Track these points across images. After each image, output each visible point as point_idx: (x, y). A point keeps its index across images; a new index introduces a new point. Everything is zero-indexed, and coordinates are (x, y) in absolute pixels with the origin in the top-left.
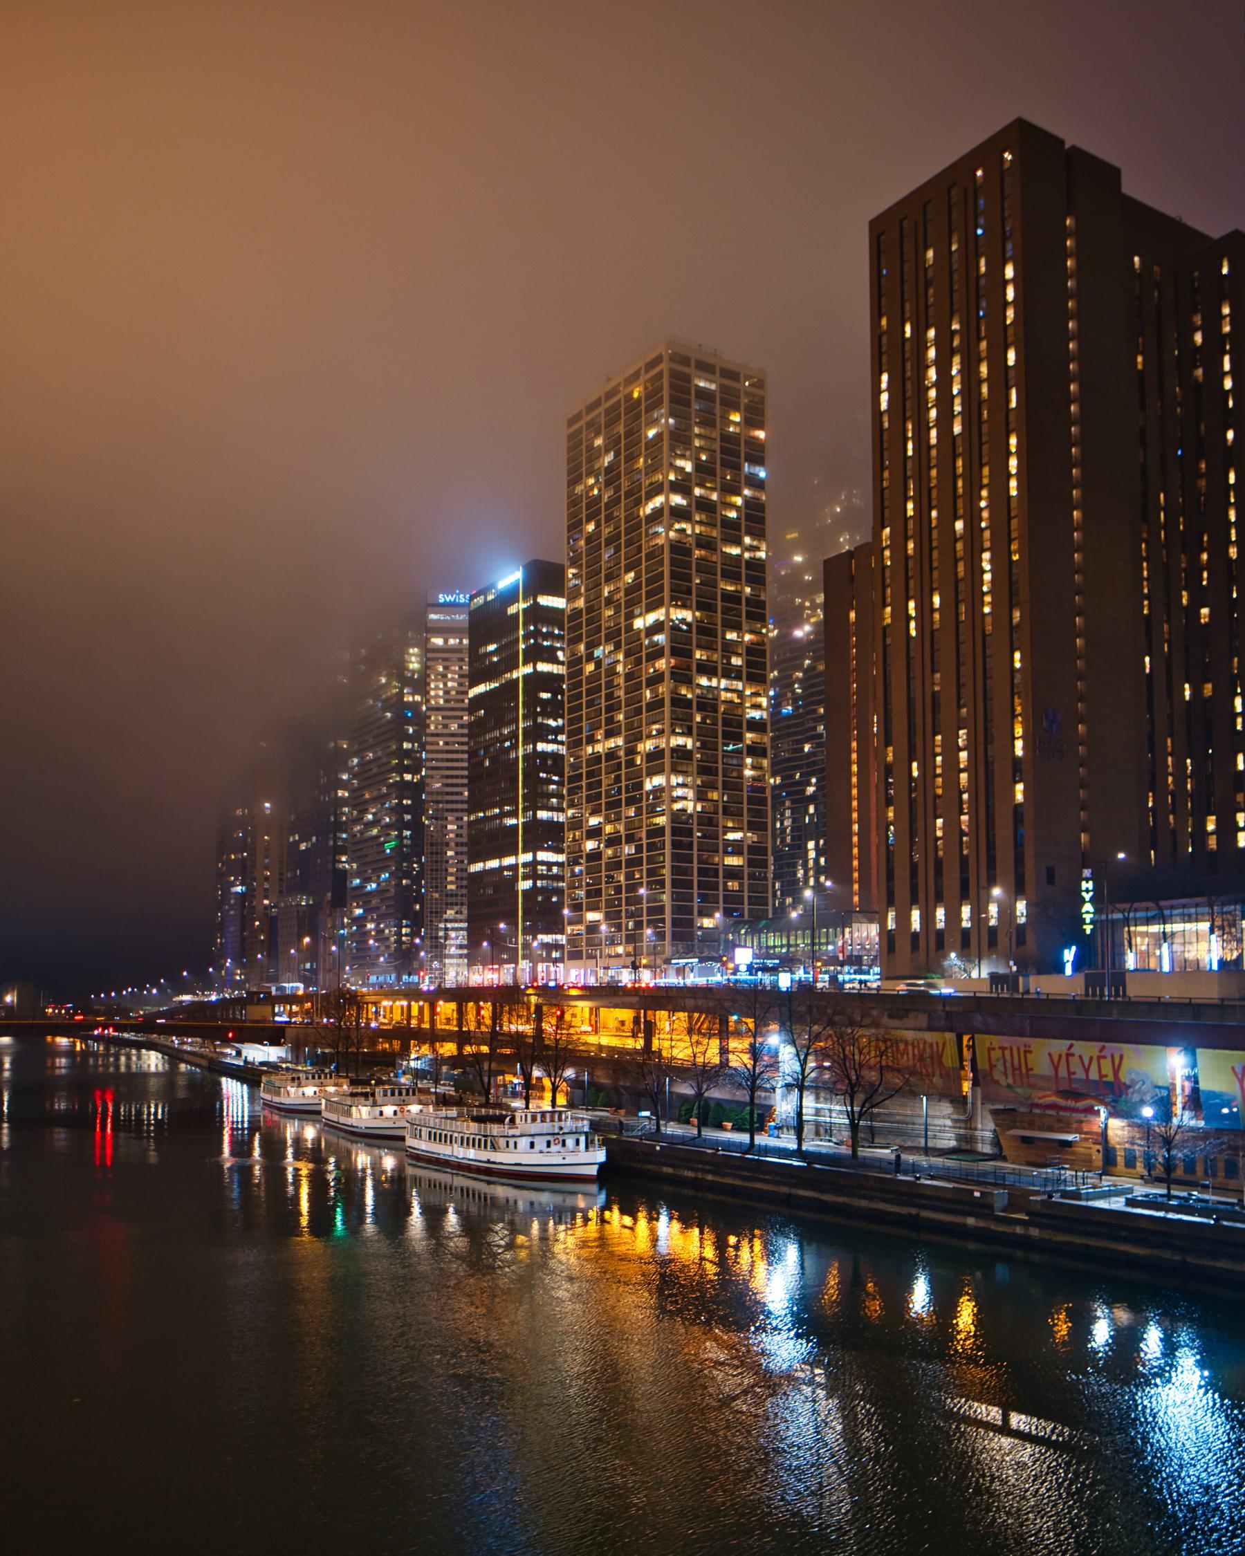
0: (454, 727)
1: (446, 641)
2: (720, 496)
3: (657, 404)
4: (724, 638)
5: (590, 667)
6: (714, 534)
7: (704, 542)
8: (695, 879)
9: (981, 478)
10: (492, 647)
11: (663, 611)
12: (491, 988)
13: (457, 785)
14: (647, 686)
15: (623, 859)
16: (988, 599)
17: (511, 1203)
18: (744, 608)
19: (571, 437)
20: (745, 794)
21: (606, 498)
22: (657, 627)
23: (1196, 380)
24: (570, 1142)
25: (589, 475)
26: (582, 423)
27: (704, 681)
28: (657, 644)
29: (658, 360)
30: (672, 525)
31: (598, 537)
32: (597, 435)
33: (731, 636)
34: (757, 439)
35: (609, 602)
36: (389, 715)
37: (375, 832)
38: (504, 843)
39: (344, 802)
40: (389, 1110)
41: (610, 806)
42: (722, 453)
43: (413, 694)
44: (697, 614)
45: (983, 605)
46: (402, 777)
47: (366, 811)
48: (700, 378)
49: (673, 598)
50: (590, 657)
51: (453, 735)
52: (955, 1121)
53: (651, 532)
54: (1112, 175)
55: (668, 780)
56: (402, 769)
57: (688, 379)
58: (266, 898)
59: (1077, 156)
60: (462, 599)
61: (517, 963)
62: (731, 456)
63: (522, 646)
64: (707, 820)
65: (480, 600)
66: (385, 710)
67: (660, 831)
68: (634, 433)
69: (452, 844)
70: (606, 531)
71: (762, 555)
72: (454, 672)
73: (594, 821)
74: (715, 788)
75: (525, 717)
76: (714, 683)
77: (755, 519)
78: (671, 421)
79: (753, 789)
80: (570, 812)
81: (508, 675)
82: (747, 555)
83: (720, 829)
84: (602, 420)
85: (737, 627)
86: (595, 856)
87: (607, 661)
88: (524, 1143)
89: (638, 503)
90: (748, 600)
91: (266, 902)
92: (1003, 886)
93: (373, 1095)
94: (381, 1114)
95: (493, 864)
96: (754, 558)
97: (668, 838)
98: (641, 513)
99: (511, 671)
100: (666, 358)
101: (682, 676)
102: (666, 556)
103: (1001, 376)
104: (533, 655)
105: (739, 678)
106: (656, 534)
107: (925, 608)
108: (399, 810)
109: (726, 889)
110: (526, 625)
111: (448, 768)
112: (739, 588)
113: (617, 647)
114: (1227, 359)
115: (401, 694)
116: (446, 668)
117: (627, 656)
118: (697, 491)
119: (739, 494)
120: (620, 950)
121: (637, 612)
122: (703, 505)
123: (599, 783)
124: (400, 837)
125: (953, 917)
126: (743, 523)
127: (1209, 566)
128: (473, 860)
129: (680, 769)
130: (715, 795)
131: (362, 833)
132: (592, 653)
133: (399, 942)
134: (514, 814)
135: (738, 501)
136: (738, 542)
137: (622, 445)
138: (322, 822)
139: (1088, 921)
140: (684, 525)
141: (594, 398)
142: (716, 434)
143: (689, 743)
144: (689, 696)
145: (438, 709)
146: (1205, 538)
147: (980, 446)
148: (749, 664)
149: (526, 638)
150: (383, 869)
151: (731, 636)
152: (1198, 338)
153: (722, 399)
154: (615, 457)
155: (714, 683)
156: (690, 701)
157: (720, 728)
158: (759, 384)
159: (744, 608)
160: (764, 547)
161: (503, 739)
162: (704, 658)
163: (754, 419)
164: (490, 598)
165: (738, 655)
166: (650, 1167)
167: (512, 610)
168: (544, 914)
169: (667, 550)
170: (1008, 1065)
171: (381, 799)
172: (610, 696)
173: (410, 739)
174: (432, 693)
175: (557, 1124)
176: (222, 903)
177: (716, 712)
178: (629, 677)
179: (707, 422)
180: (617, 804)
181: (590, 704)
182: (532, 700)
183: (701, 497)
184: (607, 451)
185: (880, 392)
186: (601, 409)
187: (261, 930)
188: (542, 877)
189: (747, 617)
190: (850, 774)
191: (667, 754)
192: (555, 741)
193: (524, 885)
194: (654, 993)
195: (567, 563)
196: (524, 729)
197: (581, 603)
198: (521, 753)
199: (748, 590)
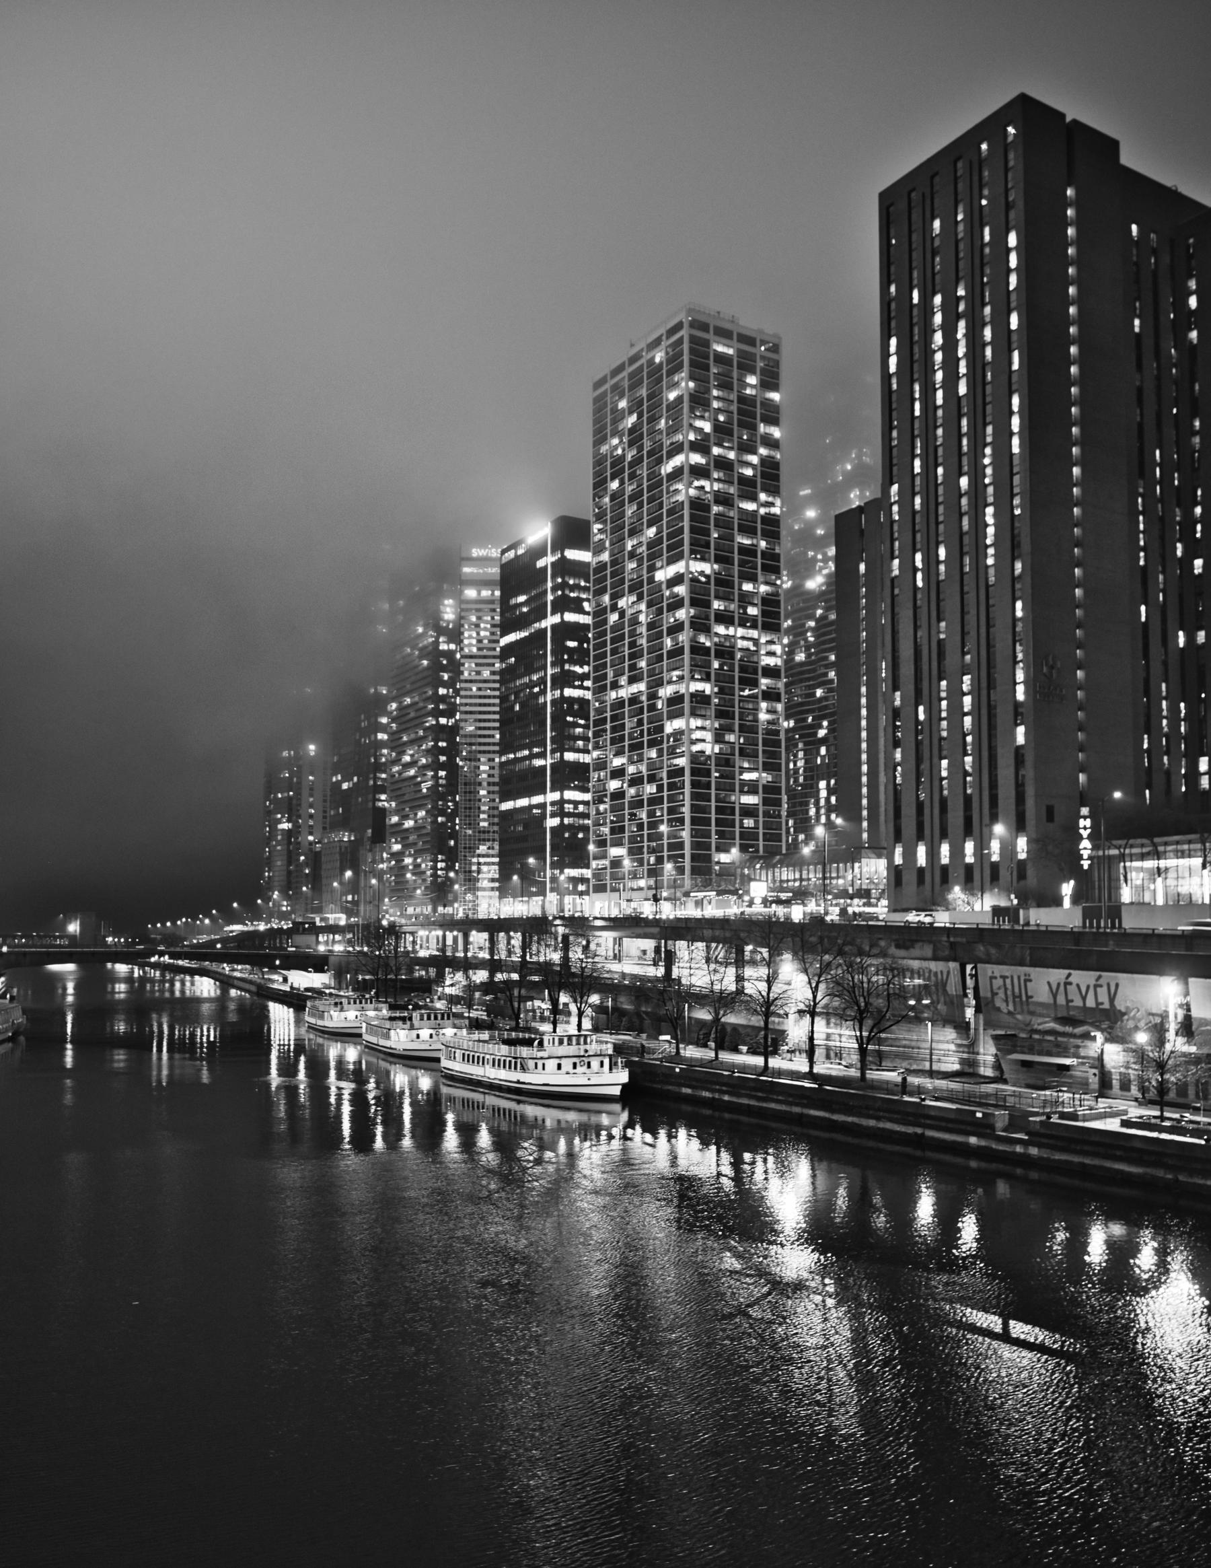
2: (737, 455)
4: (740, 589)
6: (732, 490)
7: (722, 499)
8: (713, 816)
9: (985, 436)
13: (489, 728)
15: (645, 797)
18: (759, 561)
19: (596, 400)
21: (629, 458)
23: (1191, 342)
24: (595, 1063)
25: (613, 436)
26: (607, 386)
27: (721, 629)
29: (679, 326)
30: (691, 483)
32: (621, 397)
35: (632, 555)
37: (412, 772)
38: (532, 782)
40: (425, 1033)
41: (633, 748)
43: (448, 643)
44: (716, 567)
49: (692, 552)
50: (614, 608)
51: (485, 681)
53: (672, 489)
55: (688, 723)
56: (437, 714)
57: (707, 344)
58: (311, 834)
61: (545, 895)
63: (550, 597)
64: (724, 761)
66: (421, 657)
67: (680, 772)
69: (485, 784)
70: (629, 489)
71: (776, 510)
72: (487, 622)
73: (618, 762)
74: (732, 731)
75: (553, 664)
76: (731, 631)
77: (770, 476)
79: (768, 732)
81: (537, 625)
83: (737, 770)
84: (626, 384)
85: (753, 579)
86: (619, 795)
87: (630, 612)
89: (659, 461)
93: (410, 1019)
94: (418, 1036)
95: (523, 802)
97: (687, 778)
98: (663, 472)
100: (686, 325)
101: (700, 625)
102: (686, 512)
103: (1004, 340)
104: (562, 605)
106: (677, 491)
107: (931, 561)
110: (554, 577)
112: (755, 541)
113: (640, 598)
115: (437, 643)
116: (479, 618)
117: (648, 606)
118: (716, 451)
119: (754, 452)
120: (642, 883)
121: (659, 564)
122: (722, 464)
123: (623, 726)
124: (436, 777)
126: (759, 480)
130: (731, 738)
131: (400, 773)
133: (435, 875)
134: (542, 755)
135: (754, 459)
136: (754, 498)
138: (363, 762)
139: (1085, 857)
141: (618, 363)
142: (733, 396)
143: (707, 688)
144: (708, 644)
146: (1199, 493)
147: (983, 406)
148: (764, 613)
149: (554, 589)
150: (420, 807)
151: (748, 587)
153: (738, 363)
155: (731, 631)
156: (709, 649)
158: (775, 349)
159: (759, 561)
160: (778, 502)
162: (722, 608)
164: (520, 552)
166: (670, 1087)
168: (571, 849)
170: (1009, 993)
172: (632, 645)
175: (582, 1047)
176: (270, 839)
177: (733, 658)
178: (651, 626)
179: (725, 385)
180: (639, 746)
181: (614, 652)
182: (559, 649)
184: (631, 413)
186: (625, 374)
187: (306, 864)
188: (569, 815)
189: (763, 569)
191: (687, 699)
192: (581, 687)
193: (552, 822)
195: (592, 519)
197: (605, 557)
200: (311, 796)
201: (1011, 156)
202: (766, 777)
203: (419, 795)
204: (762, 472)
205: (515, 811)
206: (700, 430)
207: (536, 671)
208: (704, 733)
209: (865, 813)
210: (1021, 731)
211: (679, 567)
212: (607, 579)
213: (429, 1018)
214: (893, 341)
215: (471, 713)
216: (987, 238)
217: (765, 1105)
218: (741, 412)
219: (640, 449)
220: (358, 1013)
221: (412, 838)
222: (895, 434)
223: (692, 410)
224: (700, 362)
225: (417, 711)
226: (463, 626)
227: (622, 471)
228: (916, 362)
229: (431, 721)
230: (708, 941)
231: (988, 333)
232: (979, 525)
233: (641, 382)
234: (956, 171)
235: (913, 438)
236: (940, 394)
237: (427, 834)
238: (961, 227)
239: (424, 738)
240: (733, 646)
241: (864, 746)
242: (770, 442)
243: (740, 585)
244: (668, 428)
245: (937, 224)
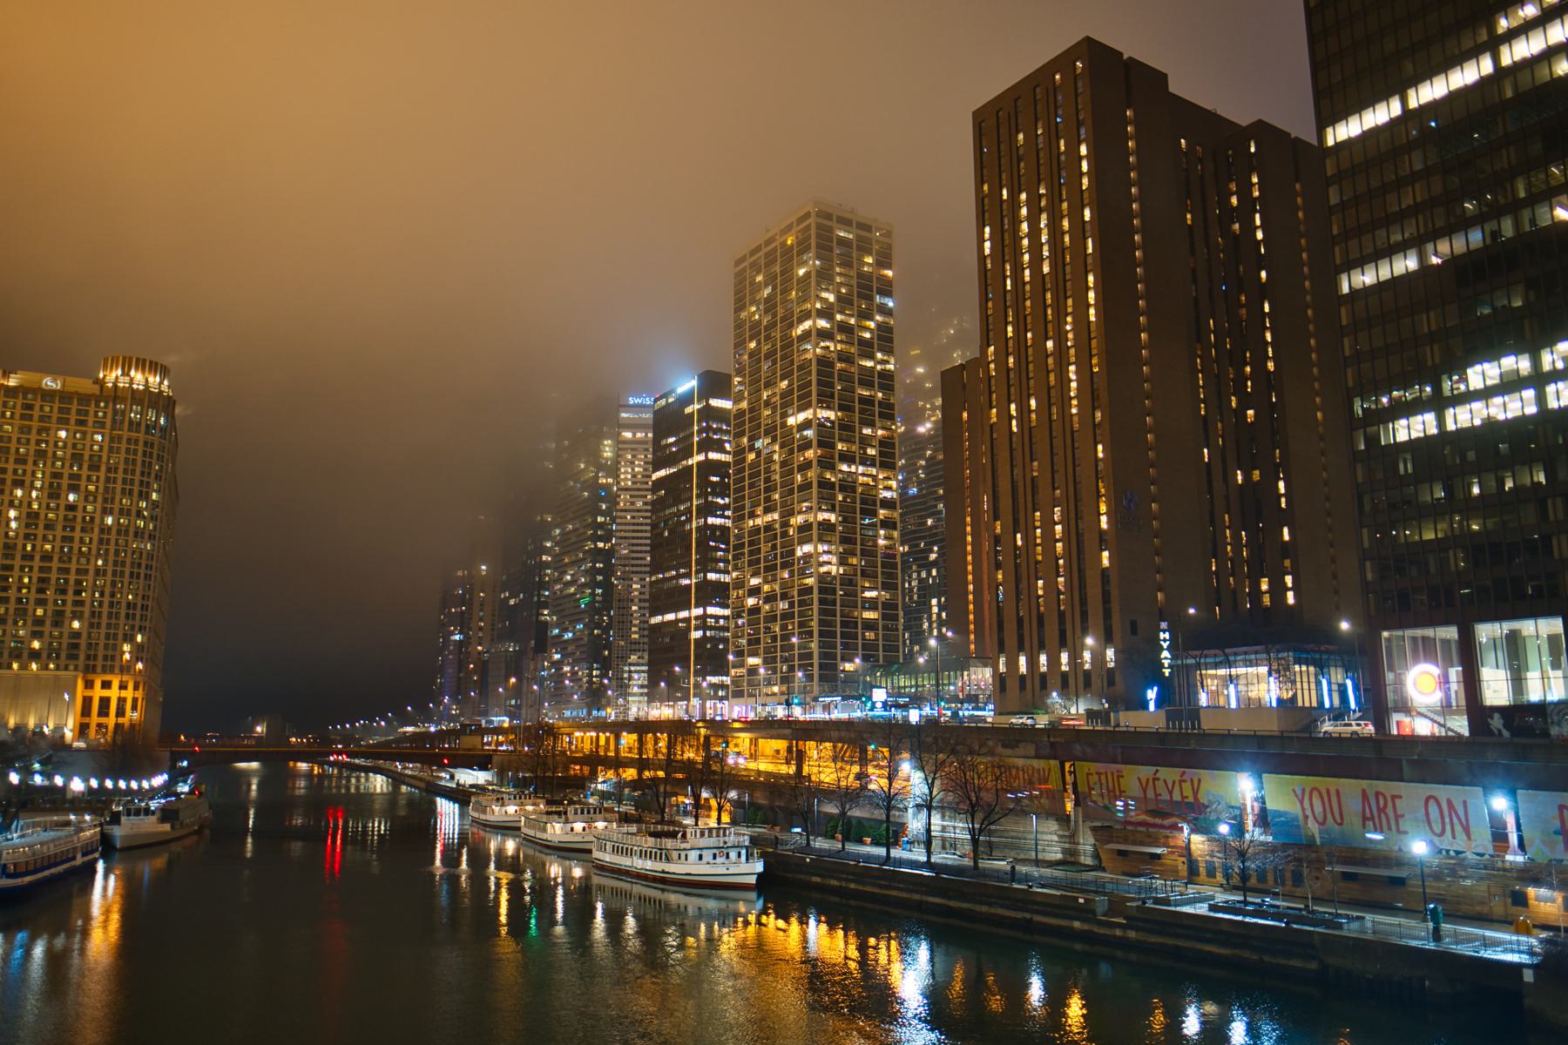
0: (639, 504)
3: (807, 249)
5: (752, 456)
7: (844, 357)
10: (672, 440)
16: (1074, 402)
19: (737, 275)
21: (765, 322)
22: (807, 424)
24: (733, 855)
25: (751, 304)
26: (746, 264)
27: (844, 468)
29: (807, 215)
32: (758, 273)
35: (767, 404)
38: (679, 599)
40: (578, 826)
41: (767, 569)
47: (565, 573)
49: (819, 401)
52: (1061, 836)
54: (1162, 78)
57: (831, 230)
59: (1133, 68)
60: (648, 401)
62: (865, 291)
63: (696, 439)
64: (848, 581)
66: (583, 490)
67: (809, 590)
68: (787, 272)
70: (765, 348)
71: (891, 367)
73: (754, 581)
76: (853, 469)
77: (885, 338)
79: (886, 556)
80: (734, 574)
85: (872, 425)
86: (755, 610)
88: (707, 855)
89: (791, 326)
95: (670, 617)
101: (827, 463)
102: (814, 368)
103: (1079, 228)
104: (705, 446)
105: (873, 465)
107: (1024, 410)
108: (593, 572)
110: (699, 421)
113: (774, 440)
115: (597, 477)
118: (839, 317)
119: (872, 319)
120: (776, 689)
122: (844, 328)
124: (593, 594)
125: (1054, 661)
128: (653, 614)
130: (854, 561)
133: (590, 682)
134: (688, 575)
135: (872, 325)
136: (872, 357)
138: (527, 578)
142: (853, 273)
143: (833, 518)
147: (1064, 283)
148: (881, 454)
149: (700, 432)
150: (578, 621)
151: (867, 431)
152: (1234, 200)
155: (853, 469)
156: (833, 484)
158: (888, 234)
163: (883, 262)
167: (688, 410)
168: (712, 659)
169: (814, 363)
172: (768, 480)
173: (603, 514)
178: (783, 464)
179: (846, 264)
180: (774, 568)
181: (751, 486)
182: (704, 483)
186: (761, 253)
187: (474, 671)
188: (711, 628)
191: (815, 527)
192: (723, 516)
197: (744, 405)
205: (663, 624)
206: (826, 300)
212: (745, 424)
214: (987, 230)
219: (774, 315)
221: (571, 648)
223: (818, 284)
224: (825, 245)
228: (1007, 245)
231: (1066, 223)
232: (1064, 381)
238: (1040, 139)
242: (886, 312)
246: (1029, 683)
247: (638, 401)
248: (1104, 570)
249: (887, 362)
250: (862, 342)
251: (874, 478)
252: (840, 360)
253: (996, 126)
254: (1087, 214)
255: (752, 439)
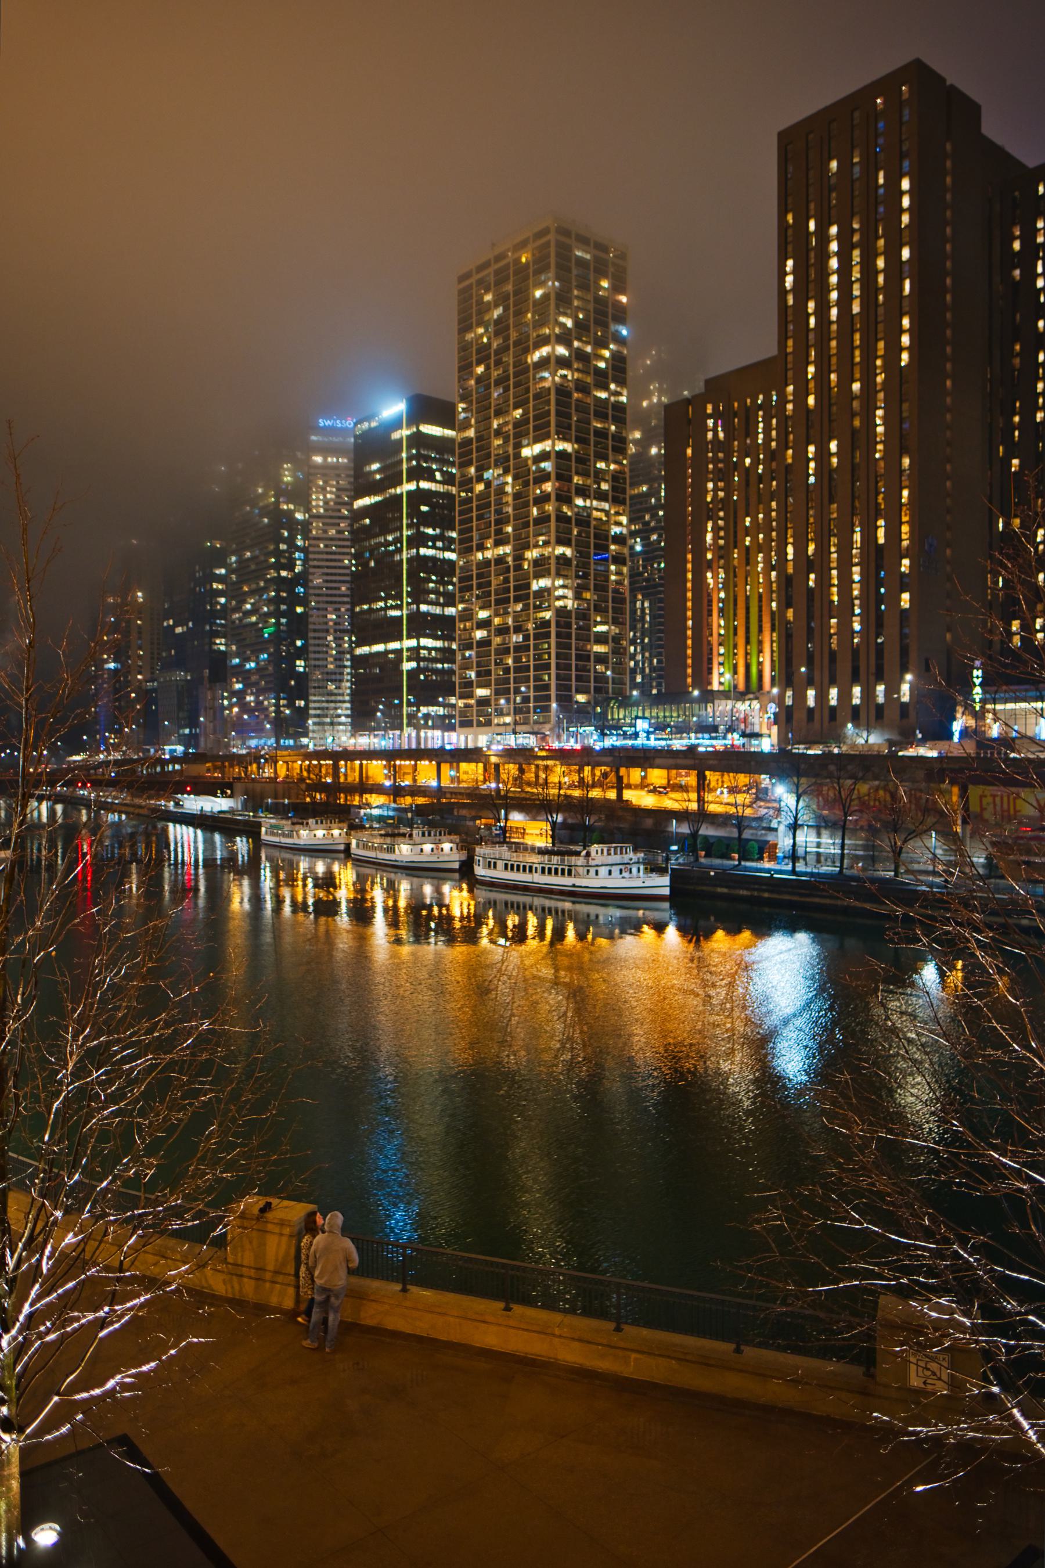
0: (332, 532)
1: (325, 459)
2: (593, 349)
4: (595, 467)
5: (480, 487)
6: (589, 380)
7: (582, 387)
8: (574, 663)
9: (876, 350)
11: (549, 442)
12: (385, 751)
13: (335, 581)
14: (534, 505)
15: (512, 645)
16: (880, 447)
17: (593, 917)
18: (610, 443)
19: (461, 292)
20: (610, 595)
21: (495, 345)
22: (544, 456)
23: (1013, 278)
24: (634, 870)
25: (479, 325)
26: (472, 280)
27: (579, 502)
28: (544, 470)
29: (545, 232)
30: (556, 371)
31: (483, 379)
32: (487, 291)
33: (601, 465)
34: (621, 302)
35: (498, 433)
36: (266, 520)
37: (254, 619)
38: (390, 630)
39: (220, 593)
40: (427, 847)
41: (498, 602)
42: (595, 312)
43: (287, 503)
44: (576, 446)
45: (875, 451)
46: (279, 574)
47: (245, 602)
48: (579, 249)
50: (480, 479)
51: (331, 539)
52: (946, 850)
53: (538, 376)
54: (973, 110)
55: (553, 583)
56: (278, 567)
57: (569, 249)
58: (140, 673)
59: (953, 92)
60: (349, 423)
61: (402, 729)
62: (600, 318)
63: (405, 466)
64: (583, 615)
65: (365, 426)
66: (262, 516)
67: (546, 623)
68: (522, 294)
69: (332, 631)
70: (495, 374)
71: (624, 399)
72: (332, 486)
73: (483, 614)
74: (589, 590)
75: (409, 527)
76: (588, 503)
78: (557, 284)
79: (616, 591)
80: (461, 607)
81: (392, 491)
82: (612, 399)
83: (592, 623)
84: (492, 279)
85: (605, 458)
86: (485, 643)
87: (496, 483)
88: (603, 871)
89: (527, 351)
90: (613, 436)
91: (139, 677)
92: (913, 672)
93: (411, 836)
94: (422, 850)
95: (379, 648)
96: (617, 402)
97: (553, 630)
98: (529, 360)
99: (395, 487)
100: (553, 230)
101: (564, 498)
102: (553, 397)
104: (415, 474)
105: (606, 500)
106: (543, 379)
107: (823, 454)
108: (277, 601)
109: (595, 671)
110: (409, 448)
111: (328, 567)
112: (606, 426)
113: (506, 471)
114: (1040, 263)
115: (277, 503)
116: (325, 482)
117: (515, 478)
118: (576, 344)
119: (607, 348)
120: (508, 720)
121: (525, 442)
122: (580, 356)
123: (489, 584)
124: (278, 624)
125: (845, 695)
126: (610, 371)
127: (1020, 426)
128: (359, 644)
129: (562, 573)
130: (587, 595)
131: (240, 620)
132: (482, 475)
133: (278, 712)
134: (399, 607)
135: (606, 354)
136: (606, 388)
137: (511, 301)
138: (199, 610)
139: (977, 700)
140: (564, 372)
141: (483, 260)
142: (590, 297)
143: (568, 552)
144: (569, 514)
145: (318, 517)
146: (1018, 405)
147: (877, 323)
148: (614, 488)
149: (409, 459)
150: (262, 651)
151: (601, 465)
152: (1017, 245)
153: (595, 267)
154: (504, 311)
155: (588, 503)
156: (570, 518)
157: (592, 541)
158: (622, 256)
159: (610, 443)
160: (625, 392)
161: (388, 544)
162: (580, 482)
163: (618, 287)
164: (374, 424)
165: (606, 481)
166: (704, 888)
168: (431, 687)
170: (998, 808)
171: (259, 592)
172: (498, 512)
173: (284, 540)
174: (314, 503)
175: (625, 856)
176: (96, 677)
177: (589, 527)
178: (517, 496)
179: (584, 287)
180: (507, 601)
181: (480, 518)
182: (414, 511)
183: (578, 349)
184: (496, 306)
185: (786, 274)
186: (491, 270)
187: (137, 700)
188: (424, 659)
189: (613, 450)
190: (686, 580)
191: (553, 561)
192: (434, 547)
193: (408, 666)
194: (631, 754)
195: (457, 399)
196: (408, 536)
197: (471, 433)
198: (404, 556)
199: (613, 428)
200: (140, 638)
201: (906, 112)
202: (615, 630)
203: (260, 640)
204: (613, 365)
205: (371, 655)
206: (563, 326)
207: (390, 532)
208: (566, 591)
209: (689, 661)
210: (906, 596)
211: (546, 445)
212: (476, 453)
213: (429, 835)
214: (790, 263)
215: (319, 567)
216: (881, 181)
217: (808, 900)
218: (596, 311)
219: (506, 339)
220: (325, 832)
221: (254, 678)
222: (790, 343)
223: (557, 307)
224: (565, 266)
225: (257, 564)
226: (311, 489)
227: (488, 357)
228: (811, 281)
229: (272, 574)
230: (669, 768)
231: (881, 263)
233: (507, 278)
234: (852, 120)
235: (808, 348)
236: (834, 312)
237: (269, 675)
238: (857, 169)
239: (265, 589)
240: (589, 516)
241: (689, 604)
242: (620, 340)
243: (595, 463)
244: (535, 322)
245: (834, 165)
246: (817, 716)
247: (328, 423)
248: (904, 611)
249: (621, 394)
250: (597, 370)
251: (607, 513)
252: (578, 390)
253: (800, 150)
254: (906, 253)
255: (481, 469)
